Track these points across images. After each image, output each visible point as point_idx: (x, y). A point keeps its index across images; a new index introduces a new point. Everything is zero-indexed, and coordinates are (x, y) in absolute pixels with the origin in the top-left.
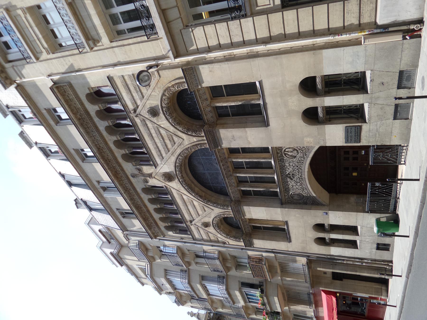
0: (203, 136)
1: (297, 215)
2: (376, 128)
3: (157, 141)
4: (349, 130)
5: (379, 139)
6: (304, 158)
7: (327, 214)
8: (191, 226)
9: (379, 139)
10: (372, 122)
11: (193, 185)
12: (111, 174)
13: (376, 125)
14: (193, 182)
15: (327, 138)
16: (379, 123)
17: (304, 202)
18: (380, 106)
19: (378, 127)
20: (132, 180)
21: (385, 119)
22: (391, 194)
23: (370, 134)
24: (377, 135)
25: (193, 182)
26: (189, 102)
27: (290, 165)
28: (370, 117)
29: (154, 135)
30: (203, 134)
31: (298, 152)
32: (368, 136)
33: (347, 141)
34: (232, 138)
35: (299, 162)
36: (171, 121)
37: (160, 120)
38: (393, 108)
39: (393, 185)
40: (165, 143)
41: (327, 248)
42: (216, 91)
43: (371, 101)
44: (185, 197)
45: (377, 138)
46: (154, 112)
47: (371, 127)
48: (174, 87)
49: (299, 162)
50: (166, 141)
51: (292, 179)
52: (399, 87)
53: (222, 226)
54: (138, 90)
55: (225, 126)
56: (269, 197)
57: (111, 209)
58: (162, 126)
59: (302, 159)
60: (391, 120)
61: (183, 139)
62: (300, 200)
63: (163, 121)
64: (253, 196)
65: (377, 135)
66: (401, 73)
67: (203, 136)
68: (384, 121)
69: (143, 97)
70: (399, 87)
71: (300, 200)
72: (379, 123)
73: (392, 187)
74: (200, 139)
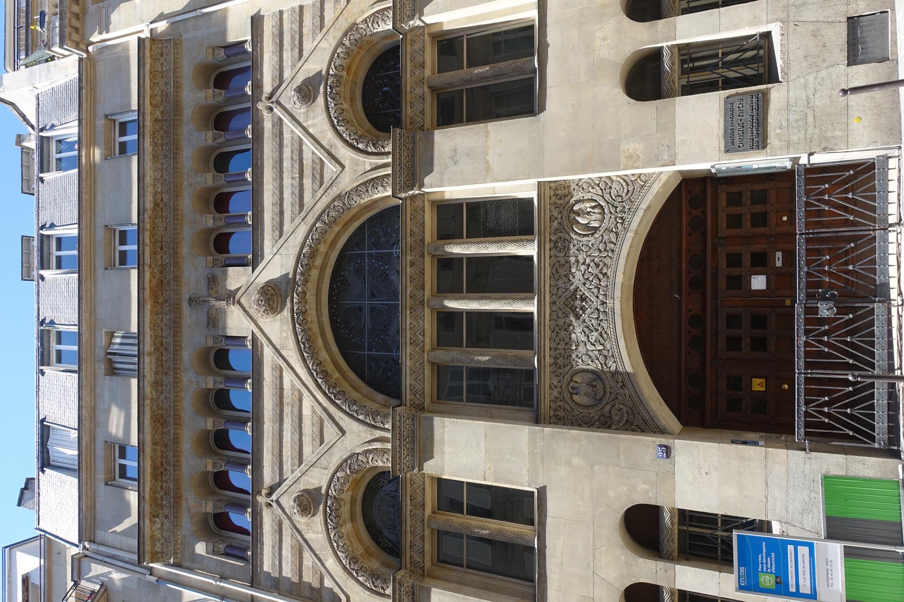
0: (387, 430)
1: (577, 461)
2: (804, 96)
3: (287, 182)
4: (736, 106)
5: (817, 131)
6: (617, 233)
7: (668, 451)
8: (265, 508)
9: (817, 131)
10: (792, 76)
11: (320, 342)
12: (147, 285)
13: (805, 86)
14: (323, 334)
15: (678, 139)
16: (811, 78)
17: (603, 408)
18: (811, 27)
19: (810, 93)
20: (185, 307)
21: (825, 65)
22: (872, 428)
23: (792, 118)
24: (810, 120)
25: (323, 334)
26: (385, 89)
27: (577, 261)
28: (787, 64)
29: (286, 164)
30: (388, 426)
31: (603, 213)
32: (785, 124)
33: (732, 145)
34: (452, 158)
35: (602, 247)
36: (332, 536)
37: (311, 115)
38: (842, 31)
39: (872, 311)
40: (301, 185)
41: (661, 565)
42: (451, 494)
43: (786, 14)
44: (288, 377)
45: (810, 130)
46: (308, 501)
47: (791, 94)
48: (366, 23)
49: (602, 247)
50: (305, 181)
51: (578, 317)
52: (853, 60)
53: (349, 525)
54: (297, 43)
55: (447, 583)
56: (505, 394)
57: (94, 102)
58: (311, 130)
59: (613, 237)
60: (843, 67)
61: (343, 167)
62: (592, 406)
63: (317, 119)
64: (465, 240)
65: (810, 120)
66: (853, 22)
67: (387, 430)
68: (824, 73)
69: (301, 463)
70: (853, 60)
71: (592, 406)
72: (811, 78)
73: (872, 396)
74: (378, 434)
